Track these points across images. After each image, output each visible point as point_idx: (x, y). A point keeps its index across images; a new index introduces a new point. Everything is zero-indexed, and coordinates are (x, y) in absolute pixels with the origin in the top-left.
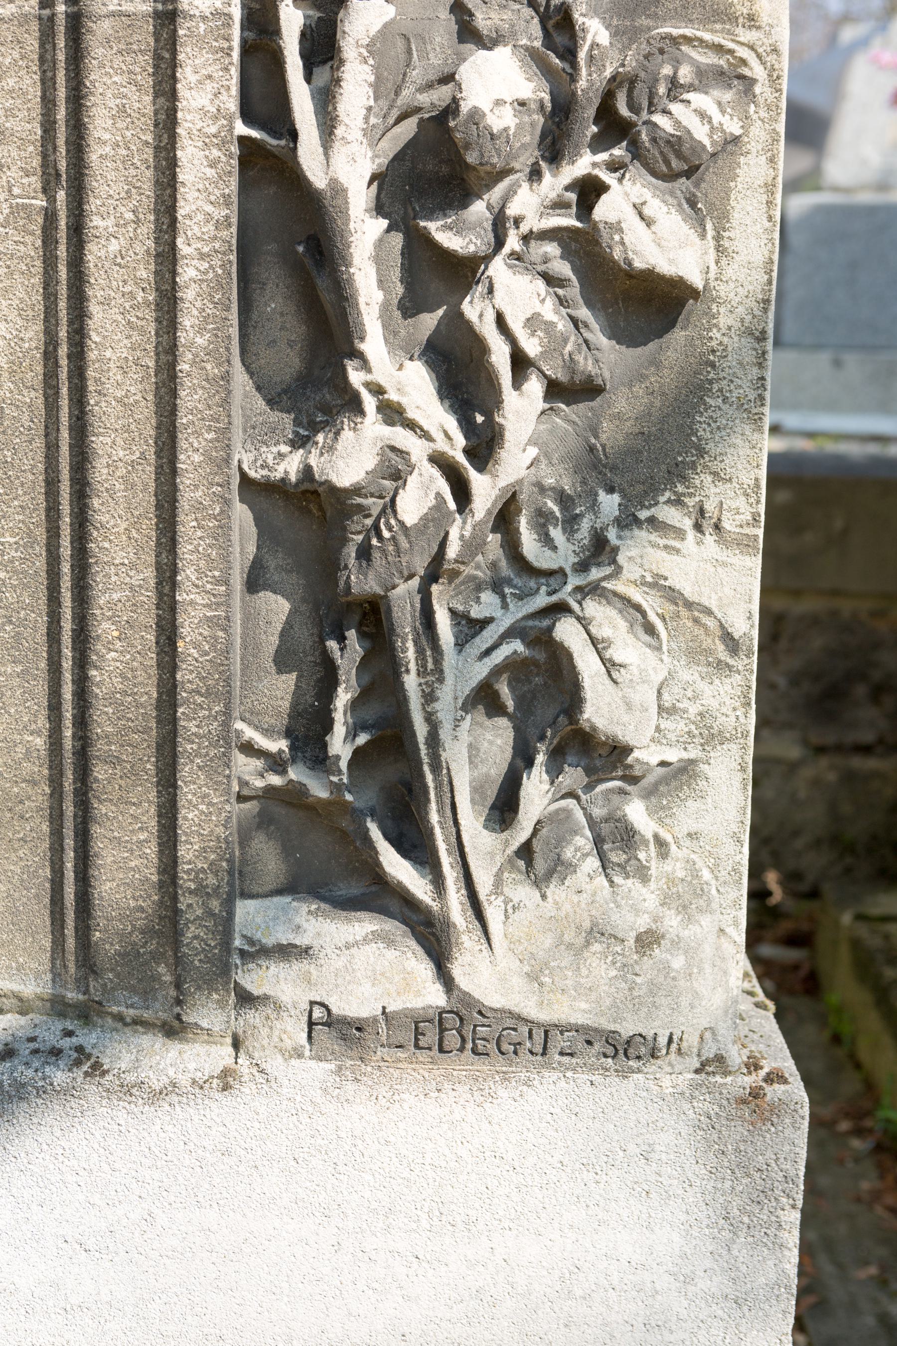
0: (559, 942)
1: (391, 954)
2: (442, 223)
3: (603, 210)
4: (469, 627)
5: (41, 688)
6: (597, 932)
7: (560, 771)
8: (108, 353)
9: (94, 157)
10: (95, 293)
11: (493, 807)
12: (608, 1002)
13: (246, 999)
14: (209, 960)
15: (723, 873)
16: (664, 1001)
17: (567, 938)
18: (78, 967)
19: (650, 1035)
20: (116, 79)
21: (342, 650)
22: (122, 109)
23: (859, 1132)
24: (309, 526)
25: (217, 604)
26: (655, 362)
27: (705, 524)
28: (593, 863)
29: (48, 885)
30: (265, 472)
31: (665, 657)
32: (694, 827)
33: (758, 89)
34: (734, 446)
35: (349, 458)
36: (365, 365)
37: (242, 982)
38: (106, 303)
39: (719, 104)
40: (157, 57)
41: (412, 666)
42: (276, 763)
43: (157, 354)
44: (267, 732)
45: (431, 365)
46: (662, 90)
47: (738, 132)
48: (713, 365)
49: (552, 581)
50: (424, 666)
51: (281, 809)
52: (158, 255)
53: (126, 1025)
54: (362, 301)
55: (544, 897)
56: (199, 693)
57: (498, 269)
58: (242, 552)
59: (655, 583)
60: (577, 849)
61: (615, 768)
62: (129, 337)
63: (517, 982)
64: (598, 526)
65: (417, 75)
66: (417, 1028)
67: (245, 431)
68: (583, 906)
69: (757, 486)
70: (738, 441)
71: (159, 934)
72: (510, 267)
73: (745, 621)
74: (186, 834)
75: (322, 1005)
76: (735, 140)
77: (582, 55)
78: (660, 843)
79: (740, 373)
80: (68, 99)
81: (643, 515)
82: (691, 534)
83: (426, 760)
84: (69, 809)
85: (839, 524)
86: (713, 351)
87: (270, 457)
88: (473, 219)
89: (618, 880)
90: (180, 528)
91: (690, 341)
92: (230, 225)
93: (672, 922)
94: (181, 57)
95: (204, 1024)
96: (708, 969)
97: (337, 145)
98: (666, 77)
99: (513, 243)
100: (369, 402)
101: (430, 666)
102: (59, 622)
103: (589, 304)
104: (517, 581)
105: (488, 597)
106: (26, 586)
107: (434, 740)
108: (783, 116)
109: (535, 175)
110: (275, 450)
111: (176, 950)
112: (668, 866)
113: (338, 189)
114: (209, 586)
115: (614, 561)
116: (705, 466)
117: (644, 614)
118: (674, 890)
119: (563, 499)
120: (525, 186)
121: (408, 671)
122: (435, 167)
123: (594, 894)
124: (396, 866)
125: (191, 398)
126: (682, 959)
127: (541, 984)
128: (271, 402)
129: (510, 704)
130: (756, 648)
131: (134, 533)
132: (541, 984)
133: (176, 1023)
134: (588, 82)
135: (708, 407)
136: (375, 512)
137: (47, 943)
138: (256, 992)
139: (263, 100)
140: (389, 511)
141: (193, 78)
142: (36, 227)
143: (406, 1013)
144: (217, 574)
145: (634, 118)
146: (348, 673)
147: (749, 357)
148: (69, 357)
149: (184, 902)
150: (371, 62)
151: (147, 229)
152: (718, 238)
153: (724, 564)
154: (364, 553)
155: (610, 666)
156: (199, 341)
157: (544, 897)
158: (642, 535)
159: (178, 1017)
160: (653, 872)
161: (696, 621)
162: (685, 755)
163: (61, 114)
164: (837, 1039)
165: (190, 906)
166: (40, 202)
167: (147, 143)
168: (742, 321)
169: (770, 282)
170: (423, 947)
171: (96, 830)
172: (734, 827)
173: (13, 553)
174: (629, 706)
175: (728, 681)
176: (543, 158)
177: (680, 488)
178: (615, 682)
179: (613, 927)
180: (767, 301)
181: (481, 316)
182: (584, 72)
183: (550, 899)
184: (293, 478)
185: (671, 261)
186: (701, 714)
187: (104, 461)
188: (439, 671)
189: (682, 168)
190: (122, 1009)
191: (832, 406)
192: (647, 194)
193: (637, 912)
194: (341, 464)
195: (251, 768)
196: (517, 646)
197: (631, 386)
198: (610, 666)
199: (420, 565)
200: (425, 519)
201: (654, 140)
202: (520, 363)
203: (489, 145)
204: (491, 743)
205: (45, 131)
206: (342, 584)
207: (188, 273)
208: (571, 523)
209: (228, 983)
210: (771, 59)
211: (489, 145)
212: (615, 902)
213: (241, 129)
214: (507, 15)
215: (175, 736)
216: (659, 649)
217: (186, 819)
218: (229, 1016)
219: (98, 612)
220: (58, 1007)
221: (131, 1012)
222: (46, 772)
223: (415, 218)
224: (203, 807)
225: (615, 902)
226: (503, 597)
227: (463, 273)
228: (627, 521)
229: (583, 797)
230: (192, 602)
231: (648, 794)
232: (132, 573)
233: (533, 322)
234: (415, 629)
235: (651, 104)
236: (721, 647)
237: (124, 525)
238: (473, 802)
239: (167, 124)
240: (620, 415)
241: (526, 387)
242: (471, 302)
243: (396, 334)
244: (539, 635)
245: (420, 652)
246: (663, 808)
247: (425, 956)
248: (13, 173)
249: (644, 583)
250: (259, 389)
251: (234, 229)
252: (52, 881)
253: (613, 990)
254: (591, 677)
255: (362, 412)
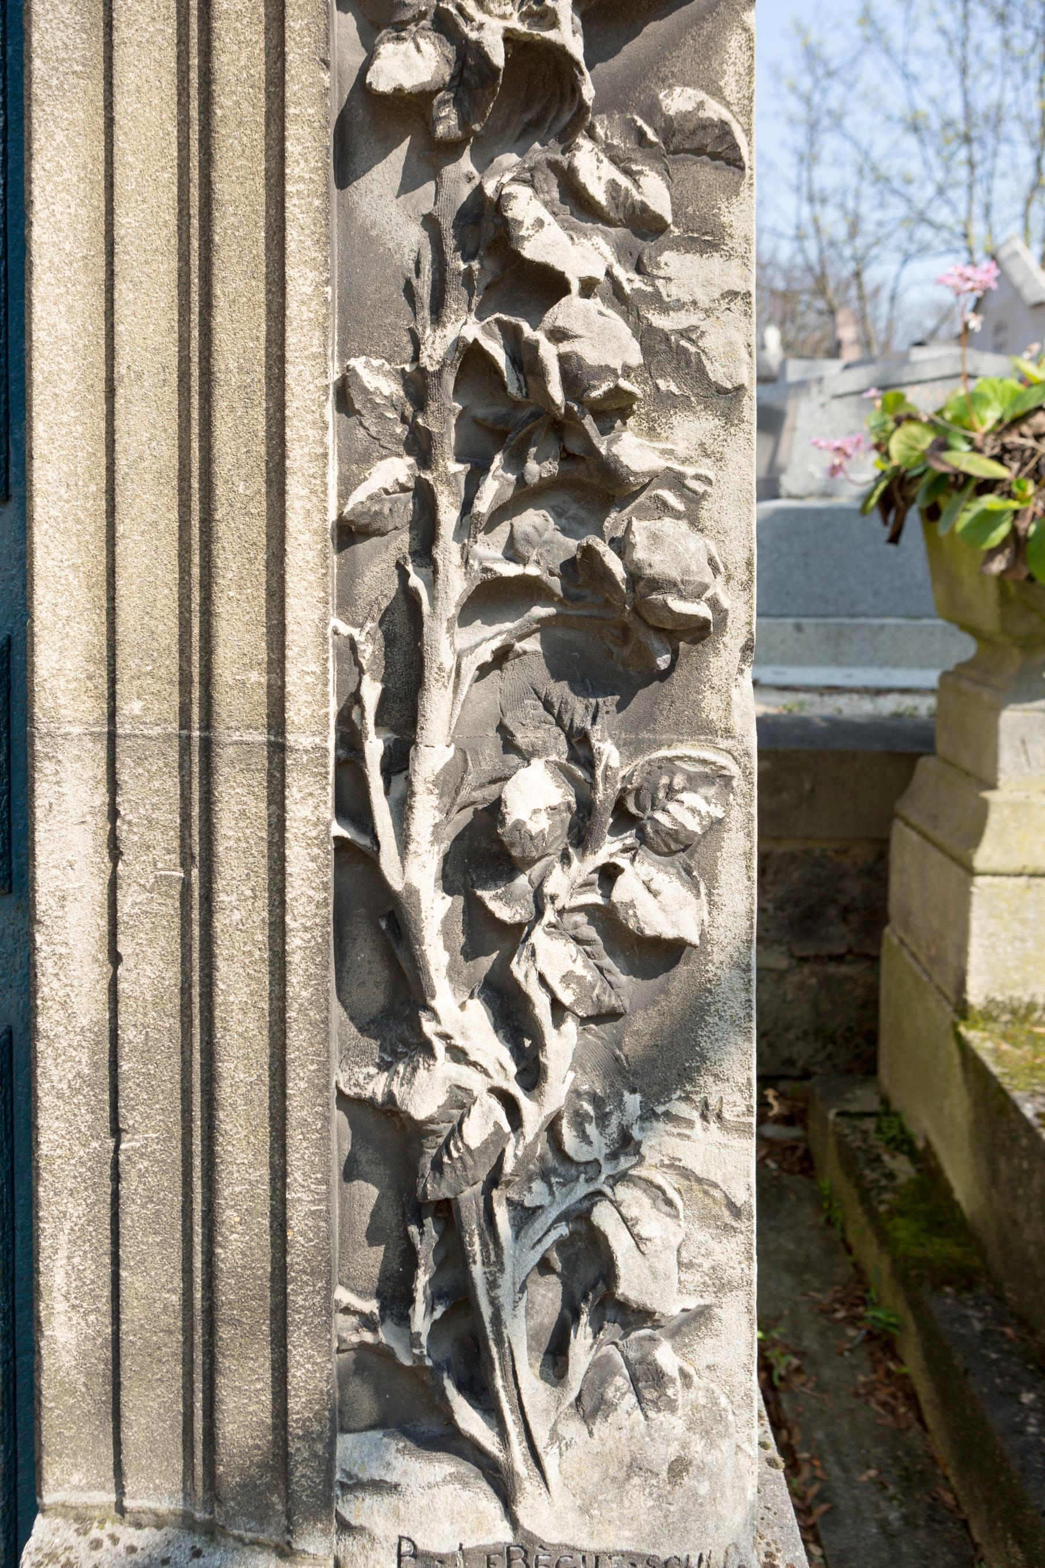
0: (605, 1476)
1: (466, 1495)
2: (493, 893)
3: (621, 891)
4: (524, 1216)
5: (176, 1255)
6: (635, 1467)
7: (601, 1328)
8: (232, 998)
9: (221, 849)
10: (222, 951)
11: (547, 1352)
12: (647, 1529)
13: (345, 1527)
14: (314, 1495)
15: (738, 1398)
16: (694, 1526)
17: (611, 1472)
18: (205, 1491)
19: (683, 1558)
20: (238, 790)
21: (422, 1234)
22: (243, 813)
23: (853, 1320)
24: (390, 1143)
25: (319, 1200)
26: (664, 991)
27: (709, 1114)
28: (631, 1399)
29: (180, 1418)
30: (357, 1090)
31: (682, 1223)
32: (711, 1361)
33: (735, 783)
34: (730, 1053)
35: (424, 1096)
36: (435, 1017)
37: (342, 1512)
38: (230, 958)
39: (706, 798)
40: (270, 776)
41: (478, 1258)
42: (368, 1322)
43: (271, 999)
44: (361, 1294)
45: (488, 1002)
46: (661, 795)
47: (721, 815)
48: (710, 991)
49: (589, 1169)
50: (488, 1257)
51: (370, 1362)
52: (271, 924)
53: (245, 1545)
54: (432, 969)
55: (591, 1433)
56: (305, 1272)
57: (539, 937)
58: (339, 1149)
59: (674, 1166)
60: (617, 1389)
61: (645, 1322)
62: (248, 985)
63: (572, 1517)
64: (624, 1123)
65: (471, 778)
66: (489, 1559)
67: (341, 1052)
68: (624, 1441)
69: (750, 1084)
70: (733, 1049)
71: (272, 1468)
72: (548, 934)
73: (744, 1188)
74: (295, 1389)
75: (409, 1540)
76: (720, 821)
77: (599, 773)
78: (684, 1375)
79: (731, 997)
80: (201, 800)
81: (660, 1109)
82: (699, 1123)
83: (491, 1336)
84: (199, 1357)
85: (807, 786)
86: (710, 981)
87: (361, 1077)
88: (518, 892)
89: (651, 1414)
90: (289, 1141)
91: (691, 974)
92: (327, 905)
93: (697, 1447)
94: (289, 780)
95: (311, 1550)
96: (728, 1492)
97: (410, 858)
98: (664, 786)
99: (550, 916)
100: (439, 1046)
101: (493, 1258)
102: (191, 1202)
103: (611, 954)
104: (561, 1170)
105: (538, 1186)
106: (165, 1172)
107: (497, 1320)
108: (756, 802)
109: (565, 859)
110: (365, 1070)
111: (287, 1487)
112: (692, 1395)
113: (412, 891)
114: (313, 1186)
115: (637, 1152)
116: (707, 1070)
117: (664, 1193)
118: (698, 1416)
119: (596, 1100)
120: (558, 866)
121: (475, 1262)
122: (484, 852)
123: (632, 1430)
124: (469, 1419)
125: (297, 1038)
126: (707, 1484)
127: (591, 1517)
128: (362, 1030)
129: (558, 1266)
130: (755, 1213)
131: (252, 1139)
132: (591, 1517)
133: (287, 1548)
134: (604, 795)
135: (707, 1024)
136: (445, 1133)
137: (179, 1466)
138: (353, 1522)
139: (352, 805)
140: (457, 1134)
141: (298, 796)
142: (176, 891)
143: (479, 1549)
144: (319, 1176)
145: (641, 815)
146: (427, 1256)
147: (738, 984)
148: (201, 995)
149: (294, 1446)
150: (436, 791)
151: (263, 902)
152: (709, 894)
153: (726, 1146)
154: (438, 1166)
155: (638, 1240)
156: (304, 994)
157: (591, 1433)
158: (660, 1126)
159: (289, 1543)
160: (680, 1402)
161: (706, 1193)
162: (702, 1302)
163: (196, 811)
164: (829, 1222)
165: (298, 1449)
166: (180, 874)
167: (262, 838)
168: (731, 957)
169: (751, 927)
170: (493, 1486)
171: (221, 1380)
172: (744, 1359)
173: (155, 1146)
174: (655, 1275)
175: (733, 1240)
176: (572, 844)
177: (688, 1088)
178: (643, 1253)
179: (650, 1462)
180: (750, 941)
181: (526, 976)
182: (601, 787)
183: (596, 1436)
184: (379, 1098)
185: (674, 924)
186: (713, 1268)
187: (228, 1082)
188: (500, 1264)
189: (677, 848)
190: (242, 1532)
191: (796, 661)
192: (653, 871)
193: (667, 1441)
194: (417, 1099)
195: (348, 1324)
196: (563, 1230)
197: (646, 1010)
198: (638, 1240)
199: (483, 1175)
200: (486, 1143)
201: (657, 832)
202: (558, 1008)
203: (529, 843)
204: (544, 1296)
205: (183, 821)
206: (420, 1190)
207: (295, 942)
208: (602, 1119)
209: (330, 1514)
210: (744, 760)
211: (529, 843)
212: (650, 1435)
213: (338, 830)
214: (541, 733)
215: (285, 1308)
216: (677, 1217)
217: (294, 1376)
218: (331, 1543)
219: (222, 1202)
220: (187, 1522)
221: (250, 1535)
222: (180, 1324)
223: (473, 886)
224: (309, 1366)
225: (650, 1435)
226: (550, 1186)
227: (514, 936)
228: (648, 1115)
229: (620, 1343)
230: (299, 1200)
231: (675, 1333)
232: (251, 1171)
233: (567, 978)
234: (479, 1225)
235: (653, 804)
236: (726, 1213)
237: (245, 1133)
238: (530, 1348)
239: (278, 826)
240: (638, 1034)
241: (563, 1028)
242: (518, 963)
243: (459, 973)
244: (580, 1216)
245: (484, 1245)
246: (685, 1345)
247: (494, 1496)
248: (158, 852)
249: (663, 1165)
250: (352, 1019)
251: (331, 908)
252: (185, 1414)
253: (651, 1518)
254: (623, 1255)
255: (433, 1056)
